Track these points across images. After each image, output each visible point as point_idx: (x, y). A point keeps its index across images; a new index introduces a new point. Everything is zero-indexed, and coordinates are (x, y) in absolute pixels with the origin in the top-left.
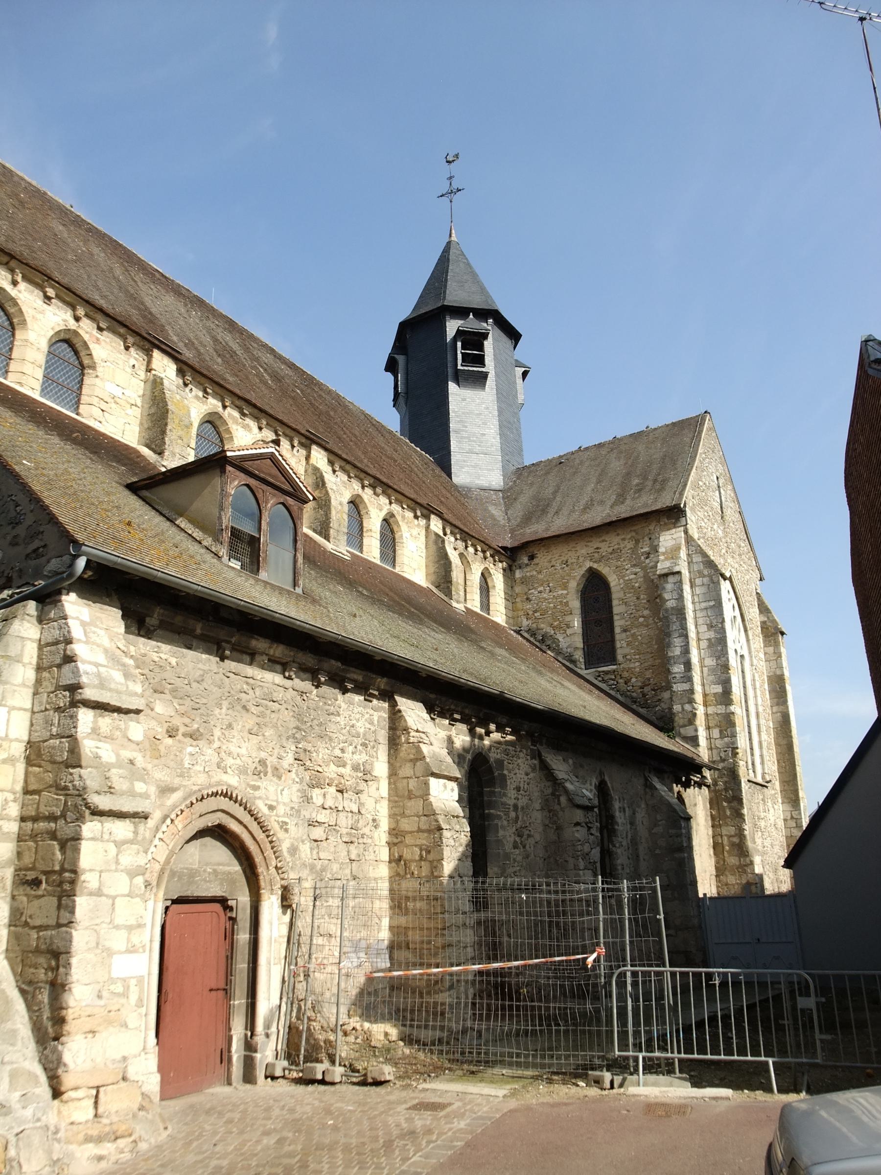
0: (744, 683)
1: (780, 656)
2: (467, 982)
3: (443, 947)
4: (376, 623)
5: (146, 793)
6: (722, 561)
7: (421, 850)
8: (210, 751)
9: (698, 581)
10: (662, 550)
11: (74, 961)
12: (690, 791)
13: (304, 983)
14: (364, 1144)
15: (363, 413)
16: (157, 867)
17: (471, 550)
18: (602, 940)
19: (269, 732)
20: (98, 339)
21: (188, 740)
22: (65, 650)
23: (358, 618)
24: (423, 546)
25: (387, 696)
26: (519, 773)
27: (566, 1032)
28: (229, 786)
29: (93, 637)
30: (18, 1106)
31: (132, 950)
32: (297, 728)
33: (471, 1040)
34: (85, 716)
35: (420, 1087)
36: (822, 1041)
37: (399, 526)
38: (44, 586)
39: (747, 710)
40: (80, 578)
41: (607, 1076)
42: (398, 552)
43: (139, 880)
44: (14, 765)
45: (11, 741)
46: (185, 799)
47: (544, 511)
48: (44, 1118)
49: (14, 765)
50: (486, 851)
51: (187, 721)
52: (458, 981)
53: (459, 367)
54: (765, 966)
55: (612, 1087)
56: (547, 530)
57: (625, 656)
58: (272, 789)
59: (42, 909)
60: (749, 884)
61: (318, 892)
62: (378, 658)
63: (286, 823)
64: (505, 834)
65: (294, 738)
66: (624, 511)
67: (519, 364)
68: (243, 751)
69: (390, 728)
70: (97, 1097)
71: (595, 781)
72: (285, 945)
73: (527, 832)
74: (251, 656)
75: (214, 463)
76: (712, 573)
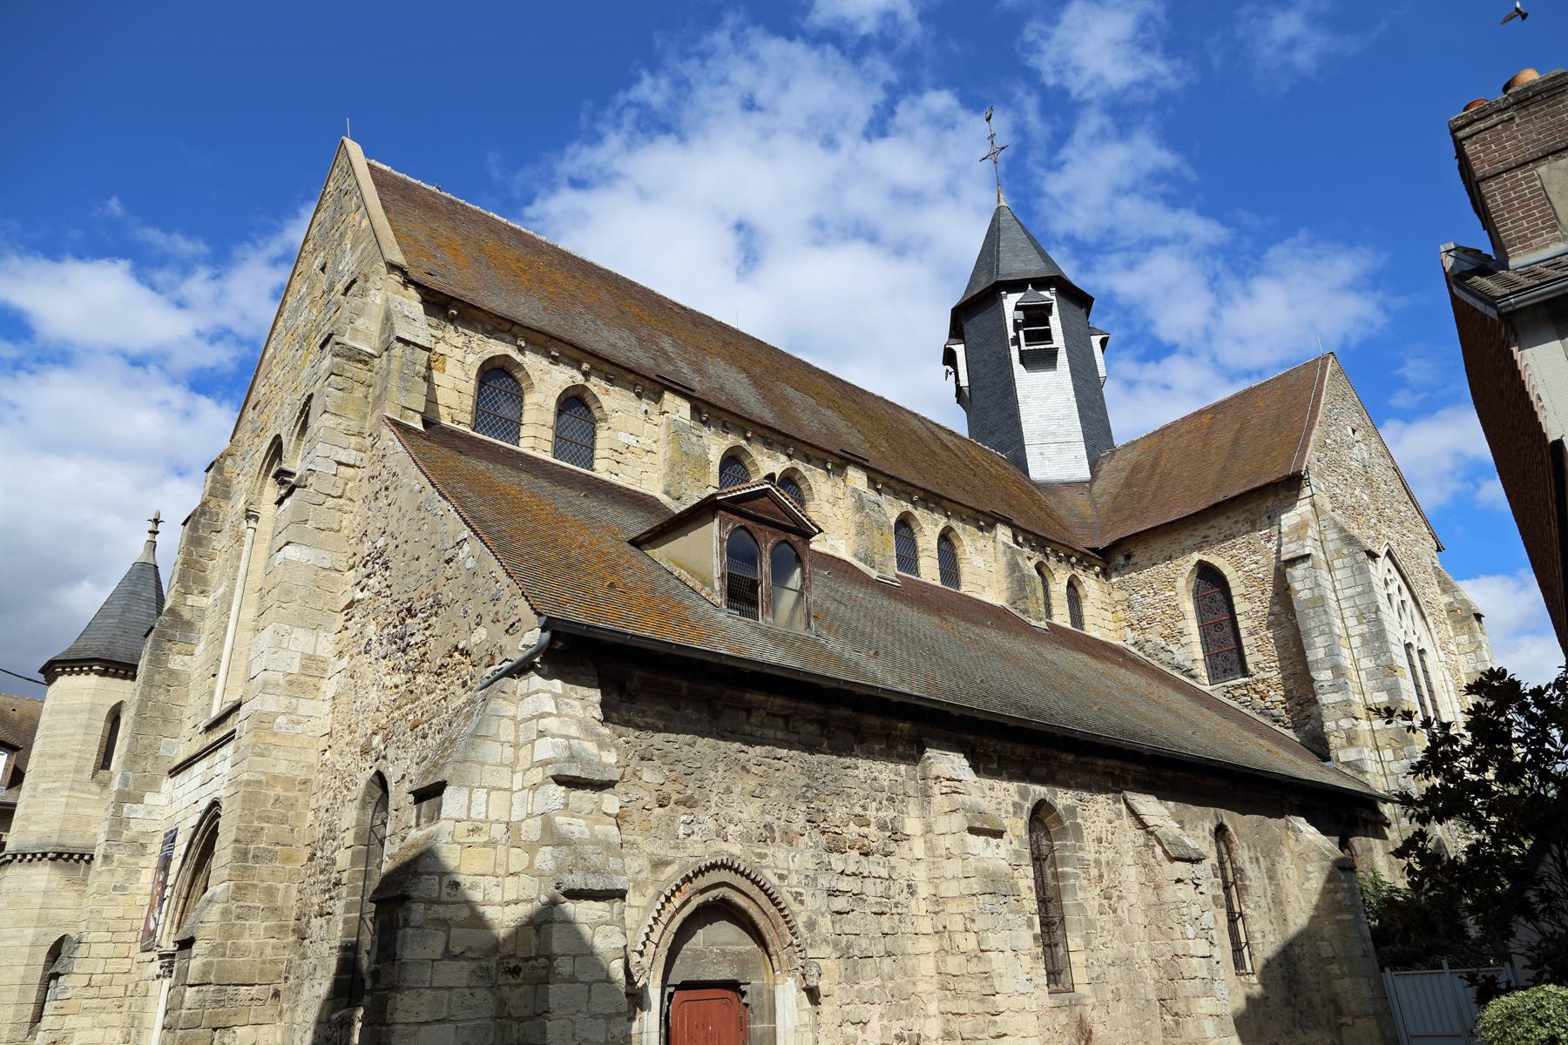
9: (1338, 563)
19: (774, 793)
21: (682, 809)
29: (566, 710)
51: (680, 787)
58: (781, 855)
68: (745, 816)
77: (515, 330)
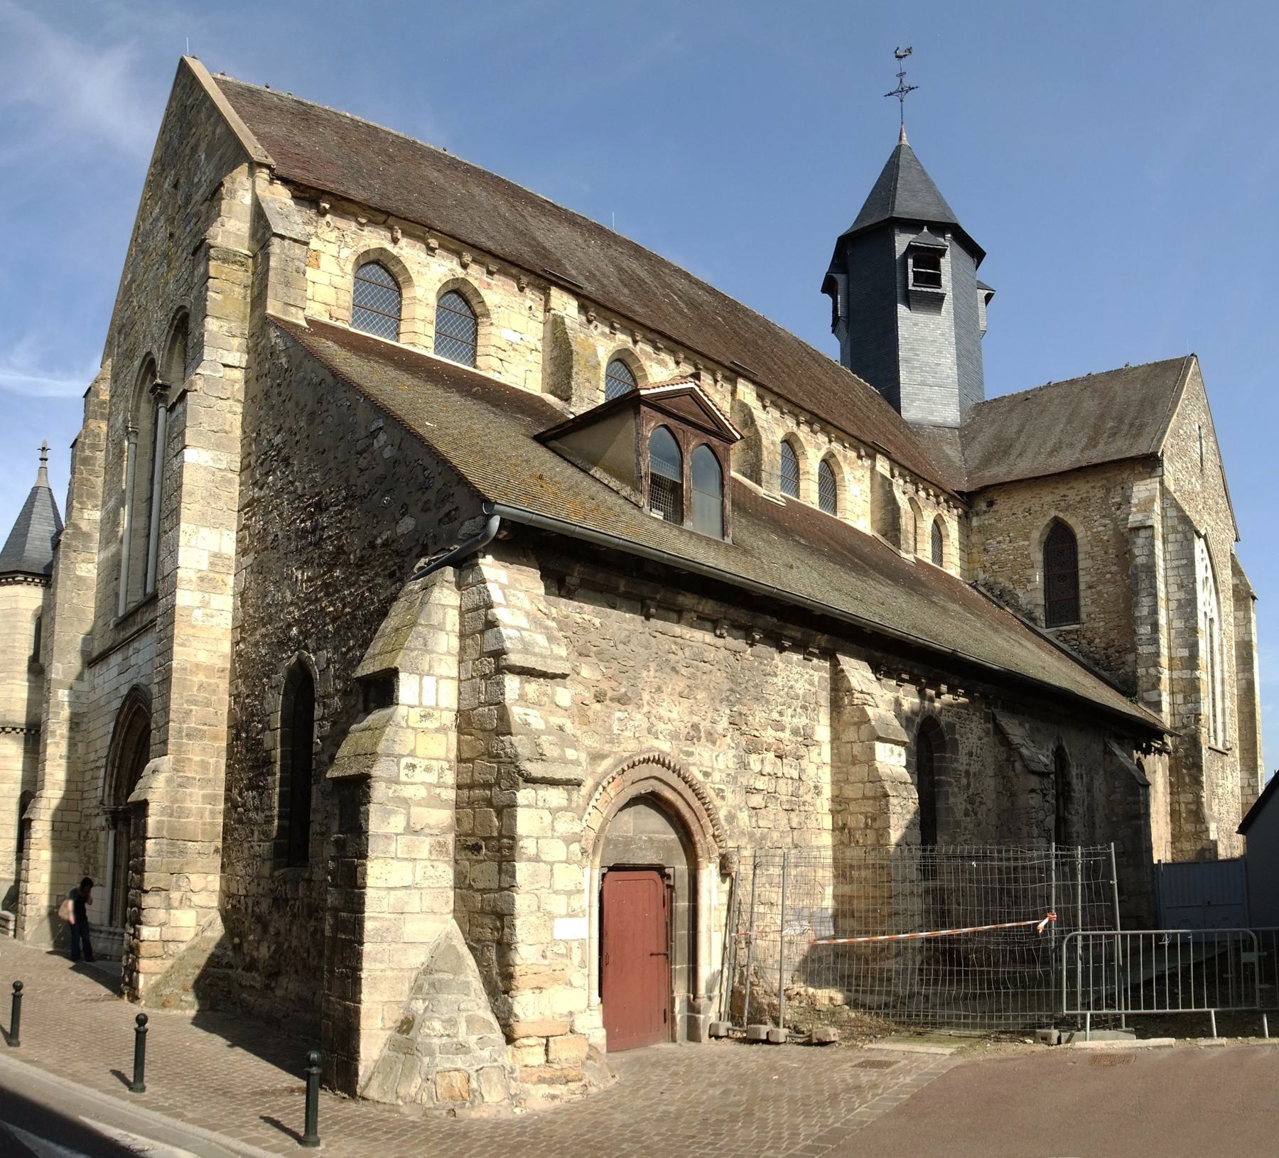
0: (1212, 648)
1: (1250, 622)
2: (914, 949)
3: (890, 916)
4: (815, 575)
5: (577, 760)
6: (1198, 517)
7: (866, 818)
8: (639, 716)
9: (1171, 537)
10: (1134, 501)
11: (518, 922)
12: (1150, 758)
13: (746, 950)
14: (809, 1096)
15: (796, 340)
16: (592, 834)
17: (922, 494)
18: (1054, 906)
19: (701, 695)
20: (489, 284)
21: (616, 705)
22: (486, 616)
23: (795, 570)
24: (868, 490)
25: (828, 654)
26: (972, 739)
27: (1015, 995)
28: (661, 752)
29: (513, 601)
30: (476, 1047)
31: (572, 914)
32: (731, 690)
33: (918, 1004)
34: (512, 683)
35: (866, 1047)
36: (1261, 990)
37: (840, 467)
38: (460, 550)
39: (1213, 676)
40: (495, 538)
41: (1055, 1033)
42: (840, 497)
43: (575, 847)
44: (446, 734)
45: (442, 710)
46: (616, 766)
47: (1006, 453)
48: (500, 1059)
49: (446, 734)
50: (935, 819)
51: (614, 684)
52: (905, 948)
53: (911, 288)
54: (1213, 927)
55: (1059, 1042)
56: (1009, 473)
57: (1089, 615)
58: (706, 755)
59: (485, 873)
60: (1203, 849)
61: (758, 860)
62: (818, 613)
63: (723, 791)
64: (956, 801)
65: (728, 700)
66: (1095, 456)
67: (981, 286)
68: (674, 715)
69: (832, 690)
70: (547, 1045)
71: (1052, 746)
72: (725, 913)
73: (978, 800)
74: (679, 614)
75: (627, 404)
76: (1186, 530)
77: (391, 221)
